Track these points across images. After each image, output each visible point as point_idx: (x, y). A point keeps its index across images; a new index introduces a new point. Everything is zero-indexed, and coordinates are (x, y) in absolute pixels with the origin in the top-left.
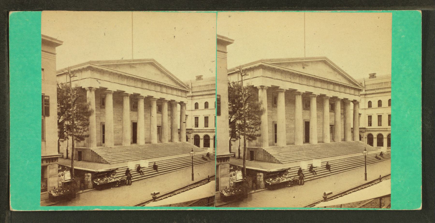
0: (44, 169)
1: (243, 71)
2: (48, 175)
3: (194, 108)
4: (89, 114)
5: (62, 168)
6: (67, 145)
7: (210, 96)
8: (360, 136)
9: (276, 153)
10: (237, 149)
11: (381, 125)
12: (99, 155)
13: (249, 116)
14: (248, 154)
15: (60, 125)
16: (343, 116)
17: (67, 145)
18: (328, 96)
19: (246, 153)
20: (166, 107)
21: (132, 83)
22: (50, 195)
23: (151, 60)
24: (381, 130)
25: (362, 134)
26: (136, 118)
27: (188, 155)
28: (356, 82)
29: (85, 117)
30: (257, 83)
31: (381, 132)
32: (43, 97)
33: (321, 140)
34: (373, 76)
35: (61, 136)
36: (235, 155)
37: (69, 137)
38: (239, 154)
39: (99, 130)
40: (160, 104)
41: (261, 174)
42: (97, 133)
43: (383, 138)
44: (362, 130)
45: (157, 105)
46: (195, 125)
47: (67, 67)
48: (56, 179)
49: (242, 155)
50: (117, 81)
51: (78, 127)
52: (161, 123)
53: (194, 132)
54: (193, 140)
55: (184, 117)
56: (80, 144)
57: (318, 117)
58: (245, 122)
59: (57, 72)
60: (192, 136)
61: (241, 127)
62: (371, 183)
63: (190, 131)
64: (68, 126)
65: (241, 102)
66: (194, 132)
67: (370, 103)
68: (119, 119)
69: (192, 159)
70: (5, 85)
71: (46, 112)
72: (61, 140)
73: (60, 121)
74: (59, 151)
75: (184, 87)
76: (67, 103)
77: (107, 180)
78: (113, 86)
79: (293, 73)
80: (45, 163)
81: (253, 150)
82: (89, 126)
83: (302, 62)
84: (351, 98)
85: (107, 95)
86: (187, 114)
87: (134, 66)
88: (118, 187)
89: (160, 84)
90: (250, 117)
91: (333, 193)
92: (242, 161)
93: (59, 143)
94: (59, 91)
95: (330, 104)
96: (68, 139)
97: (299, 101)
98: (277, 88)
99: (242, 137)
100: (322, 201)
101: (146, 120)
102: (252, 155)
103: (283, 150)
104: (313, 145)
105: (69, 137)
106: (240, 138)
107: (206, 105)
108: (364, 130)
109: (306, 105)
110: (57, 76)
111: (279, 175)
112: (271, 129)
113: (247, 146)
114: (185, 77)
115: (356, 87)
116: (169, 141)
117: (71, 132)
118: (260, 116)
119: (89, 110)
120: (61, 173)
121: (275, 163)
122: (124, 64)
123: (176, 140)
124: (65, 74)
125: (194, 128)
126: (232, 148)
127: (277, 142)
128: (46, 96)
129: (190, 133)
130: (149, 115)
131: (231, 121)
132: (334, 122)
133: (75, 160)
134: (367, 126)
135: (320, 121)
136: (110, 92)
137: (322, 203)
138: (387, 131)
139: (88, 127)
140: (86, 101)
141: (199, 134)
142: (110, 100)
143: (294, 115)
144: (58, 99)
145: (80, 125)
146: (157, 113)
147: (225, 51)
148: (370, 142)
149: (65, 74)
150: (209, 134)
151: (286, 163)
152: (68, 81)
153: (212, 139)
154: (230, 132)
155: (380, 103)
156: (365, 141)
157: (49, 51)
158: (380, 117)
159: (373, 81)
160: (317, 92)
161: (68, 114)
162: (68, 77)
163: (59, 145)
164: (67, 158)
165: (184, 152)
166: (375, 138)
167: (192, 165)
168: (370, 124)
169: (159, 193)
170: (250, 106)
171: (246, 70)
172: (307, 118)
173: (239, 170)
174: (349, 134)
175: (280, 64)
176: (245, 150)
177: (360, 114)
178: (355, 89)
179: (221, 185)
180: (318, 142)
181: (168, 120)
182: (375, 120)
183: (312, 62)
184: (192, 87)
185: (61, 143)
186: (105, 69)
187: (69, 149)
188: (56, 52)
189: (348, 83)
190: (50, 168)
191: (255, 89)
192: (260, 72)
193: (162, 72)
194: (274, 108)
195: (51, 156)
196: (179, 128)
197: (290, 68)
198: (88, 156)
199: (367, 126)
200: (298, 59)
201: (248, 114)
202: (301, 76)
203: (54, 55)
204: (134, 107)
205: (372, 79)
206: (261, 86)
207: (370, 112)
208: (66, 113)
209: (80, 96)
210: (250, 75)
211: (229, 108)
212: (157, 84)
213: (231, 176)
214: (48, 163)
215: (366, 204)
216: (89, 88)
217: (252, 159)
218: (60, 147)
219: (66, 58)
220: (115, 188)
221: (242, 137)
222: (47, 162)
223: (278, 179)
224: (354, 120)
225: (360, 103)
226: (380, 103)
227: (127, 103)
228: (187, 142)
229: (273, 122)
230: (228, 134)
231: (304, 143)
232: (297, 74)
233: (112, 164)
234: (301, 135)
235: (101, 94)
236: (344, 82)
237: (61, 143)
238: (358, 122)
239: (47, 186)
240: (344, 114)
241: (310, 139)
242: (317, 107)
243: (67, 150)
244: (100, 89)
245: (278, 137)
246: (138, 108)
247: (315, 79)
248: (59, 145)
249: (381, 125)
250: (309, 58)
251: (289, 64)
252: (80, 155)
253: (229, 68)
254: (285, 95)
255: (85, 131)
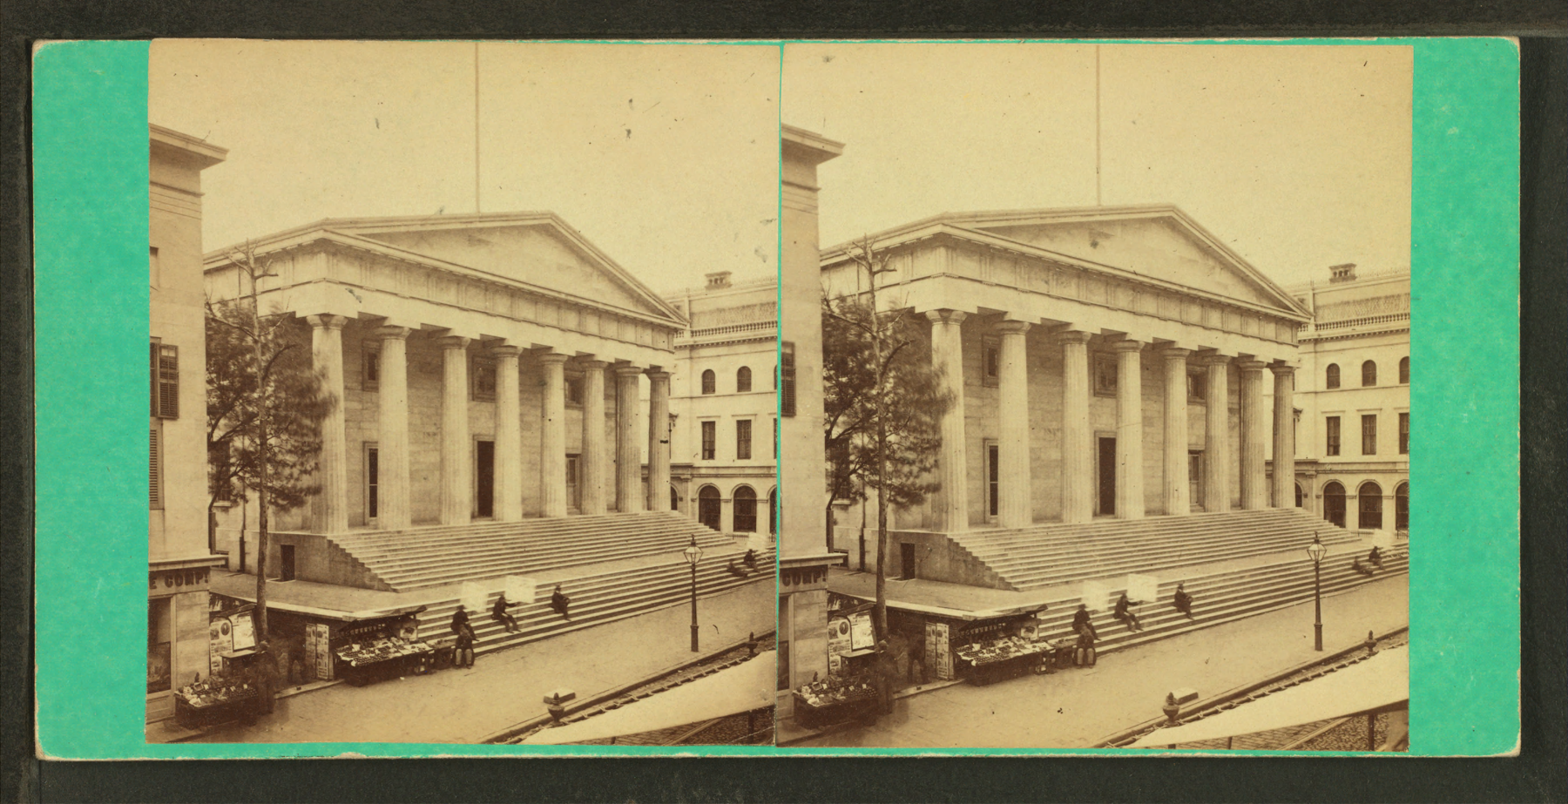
0: (158, 608)
1: (875, 257)
2: (173, 630)
3: (698, 390)
4: (320, 410)
5: (223, 606)
6: (243, 521)
7: (758, 347)
8: (1298, 489)
9: (995, 550)
10: (856, 536)
11: (1373, 452)
12: (356, 560)
13: (897, 417)
14: (893, 556)
15: (218, 450)
16: (1236, 419)
17: (243, 521)
18: (1180, 345)
19: (887, 551)
20: (597, 385)
21: (476, 300)
22: (181, 702)
23: (543, 215)
24: (1373, 467)
25: (1304, 483)
26: (491, 424)
27: (677, 558)
28: (1284, 295)
29: (307, 422)
30: (925, 300)
31: (1372, 477)
32: (155, 348)
33: (1156, 505)
34: (1343, 274)
35: (221, 489)
36: (846, 559)
37: (250, 494)
38: (863, 554)
39: (358, 467)
40: (577, 374)
41: (323, 628)
42: (349, 480)
43: (1379, 498)
44: (1304, 468)
45: (566, 380)
46: (704, 450)
47: (240, 240)
48: (202, 645)
49: (871, 559)
50: (422, 292)
51: (280, 457)
52: (579, 444)
53: (701, 476)
54: (697, 505)
55: (663, 422)
56: (287, 519)
57: (1147, 421)
58: (263, 443)
59: (207, 260)
60: (691, 490)
61: (869, 458)
62: (1338, 660)
63: (686, 474)
64: (244, 455)
65: (871, 367)
66: (701, 476)
67: (1333, 371)
68: (1048, 422)
69: (694, 572)
70: (18, 306)
71: (165, 404)
72: (220, 503)
73: (217, 435)
74: (211, 545)
75: (664, 314)
76: (242, 370)
77: (385, 650)
78: (408, 309)
79: (1056, 262)
80: (162, 589)
81: (911, 541)
82: (323, 455)
83: (1089, 223)
84: (1266, 353)
85: (386, 343)
86: (673, 411)
87: (484, 237)
88: (425, 673)
89: (577, 304)
90: (282, 424)
91: (1201, 697)
92: (872, 581)
93: (211, 517)
94: (214, 328)
95: (1190, 374)
96: (246, 501)
97: (1078, 363)
98: (999, 316)
99: (872, 494)
100: (1160, 725)
101: (527, 434)
102: (909, 558)
103: (1019, 541)
104: (1128, 524)
105: (250, 494)
106: (865, 499)
107: (744, 379)
108: (1311, 470)
109: (1103, 379)
110: (207, 273)
111: (1004, 630)
112: (978, 464)
113: (891, 527)
114: (667, 278)
115: (1283, 314)
116: (610, 509)
117: (257, 475)
118: (937, 420)
119: (320, 396)
120: (219, 624)
121: (992, 587)
122: (448, 232)
123: (635, 505)
124: (233, 265)
125: (699, 462)
126: (836, 535)
127: (1000, 511)
128: (167, 347)
129: (686, 480)
130: (539, 413)
131: (834, 435)
132: (1202, 442)
133: (270, 576)
134: (1321, 454)
135: (1155, 436)
136: (395, 331)
137: (1160, 731)
138: (1396, 471)
139: (317, 456)
140: (310, 364)
141: (719, 483)
142: (395, 360)
143: (1060, 414)
144: (209, 355)
145: (290, 452)
146: (567, 407)
147: (810, 184)
148: (1335, 512)
149: (233, 265)
150: (752, 482)
151: (1030, 589)
152: (247, 291)
153: (762, 501)
154: (828, 474)
155: (1369, 373)
156: (1315, 509)
157: (176, 185)
158: (1369, 421)
159: (1344, 292)
160: (1143, 331)
161: (245, 412)
162: (246, 276)
163: (212, 523)
164: (243, 569)
165: (662, 549)
166: (1353, 497)
167: (694, 596)
168: (1334, 447)
169: (571, 697)
170: (901, 381)
171: (888, 251)
172: (1106, 424)
173: (861, 614)
174: (1259, 483)
175: (1009, 230)
176: (882, 541)
177: (1297, 412)
178: (1279, 321)
179: (798, 667)
180: (1148, 513)
181: (608, 434)
182: (1351, 434)
183: (1124, 224)
184: (691, 314)
185: (220, 517)
186: (379, 248)
187: (248, 538)
188: (203, 189)
189: (1254, 301)
190: (180, 607)
191: (920, 322)
192: (936, 261)
193: (583, 258)
194: (987, 390)
195: (184, 562)
196: (645, 461)
197: (1044, 243)
198: (318, 563)
199: (1321, 454)
200: (1073, 212)
201: (895, 413)
202: (1084, 274)
203: (195, 200)
204: (484, 386)
205: (1340, 285)
206: (941, 311)
207: (1334, 403)
208: (238, 409)
209: (288, 347)
210: (901, 269)
211: (826, 389)
212: (566, 302)
213: (833, 634)
214: (173, 589)
215: (1320, 736)
216: (322, 316)
217: (908, 573)
218: (218, 530)
219: (236, 208)
220: (1035, 677)
221: (872, 494)
222: (169, 585)
223: (1001, 645)
224: (1275, 434)
225: (1296, 372)
226: (1369, 373)
227: (457, 369)
228: (675, 513)
229: (985, 440)
230: (823, 483)
231: (1095, 515)
232: (1071, 266)
233: (1023, 590)
234: (1084, 487)
235: (365, 339)
236: (1238, 294)
237: (220, 516)
238: (1289, 441)
239: (168, 671)
240: (1240, 411)
241: (1118, 503)
242: (1143, 386)
243: (242, 542)
244: (360, 320)
245: (1000, 494)
246: (499, 389)
247: (1137, 286)
248: (212, 523)
249: (1373, 452)
250: (1112, 211)
251: (1041, 230)
252: (288, 559)
253: (826, 244)
254: (1028, 341)
255: (305, 472)
